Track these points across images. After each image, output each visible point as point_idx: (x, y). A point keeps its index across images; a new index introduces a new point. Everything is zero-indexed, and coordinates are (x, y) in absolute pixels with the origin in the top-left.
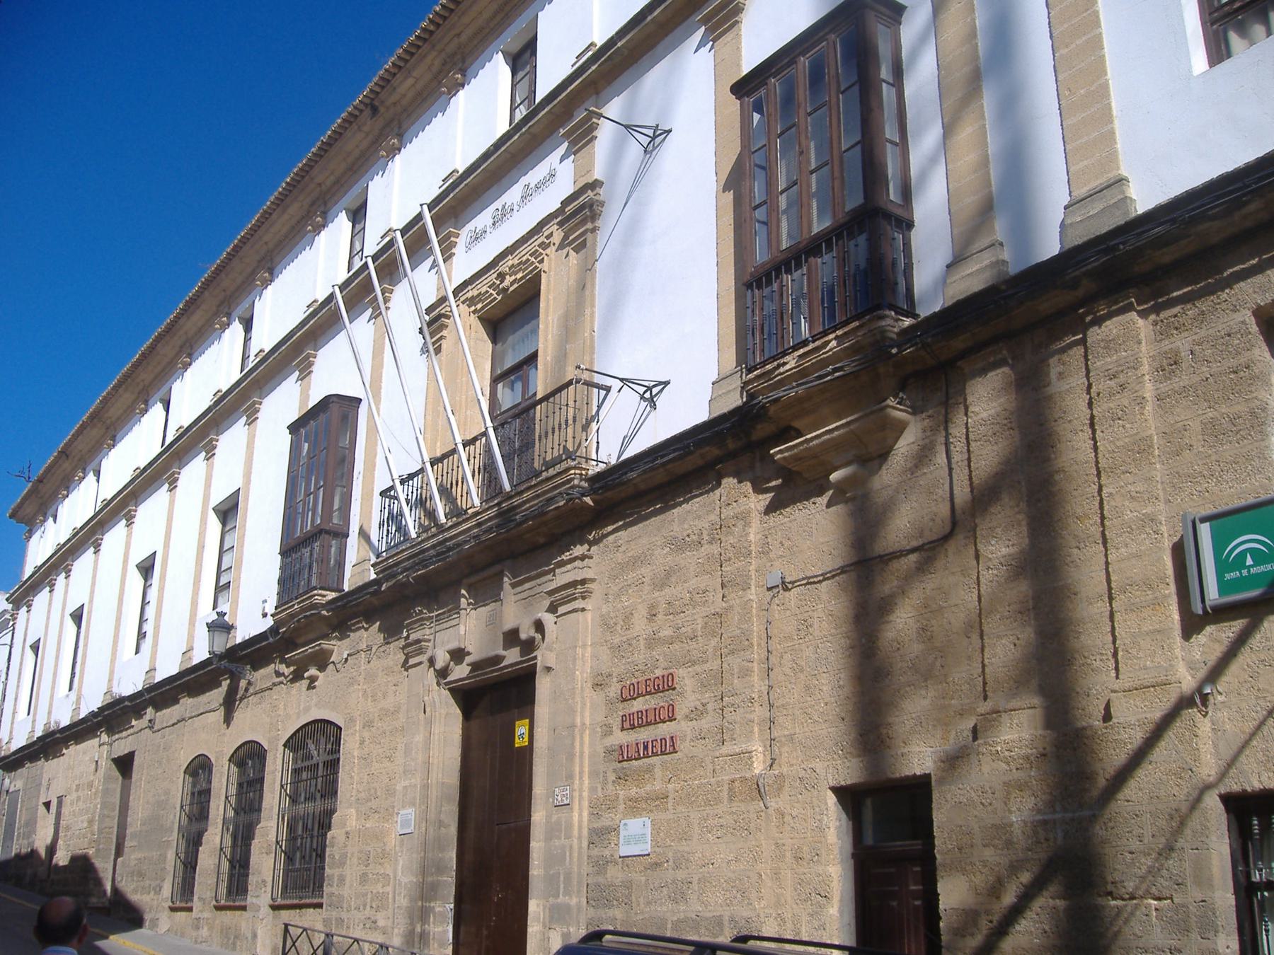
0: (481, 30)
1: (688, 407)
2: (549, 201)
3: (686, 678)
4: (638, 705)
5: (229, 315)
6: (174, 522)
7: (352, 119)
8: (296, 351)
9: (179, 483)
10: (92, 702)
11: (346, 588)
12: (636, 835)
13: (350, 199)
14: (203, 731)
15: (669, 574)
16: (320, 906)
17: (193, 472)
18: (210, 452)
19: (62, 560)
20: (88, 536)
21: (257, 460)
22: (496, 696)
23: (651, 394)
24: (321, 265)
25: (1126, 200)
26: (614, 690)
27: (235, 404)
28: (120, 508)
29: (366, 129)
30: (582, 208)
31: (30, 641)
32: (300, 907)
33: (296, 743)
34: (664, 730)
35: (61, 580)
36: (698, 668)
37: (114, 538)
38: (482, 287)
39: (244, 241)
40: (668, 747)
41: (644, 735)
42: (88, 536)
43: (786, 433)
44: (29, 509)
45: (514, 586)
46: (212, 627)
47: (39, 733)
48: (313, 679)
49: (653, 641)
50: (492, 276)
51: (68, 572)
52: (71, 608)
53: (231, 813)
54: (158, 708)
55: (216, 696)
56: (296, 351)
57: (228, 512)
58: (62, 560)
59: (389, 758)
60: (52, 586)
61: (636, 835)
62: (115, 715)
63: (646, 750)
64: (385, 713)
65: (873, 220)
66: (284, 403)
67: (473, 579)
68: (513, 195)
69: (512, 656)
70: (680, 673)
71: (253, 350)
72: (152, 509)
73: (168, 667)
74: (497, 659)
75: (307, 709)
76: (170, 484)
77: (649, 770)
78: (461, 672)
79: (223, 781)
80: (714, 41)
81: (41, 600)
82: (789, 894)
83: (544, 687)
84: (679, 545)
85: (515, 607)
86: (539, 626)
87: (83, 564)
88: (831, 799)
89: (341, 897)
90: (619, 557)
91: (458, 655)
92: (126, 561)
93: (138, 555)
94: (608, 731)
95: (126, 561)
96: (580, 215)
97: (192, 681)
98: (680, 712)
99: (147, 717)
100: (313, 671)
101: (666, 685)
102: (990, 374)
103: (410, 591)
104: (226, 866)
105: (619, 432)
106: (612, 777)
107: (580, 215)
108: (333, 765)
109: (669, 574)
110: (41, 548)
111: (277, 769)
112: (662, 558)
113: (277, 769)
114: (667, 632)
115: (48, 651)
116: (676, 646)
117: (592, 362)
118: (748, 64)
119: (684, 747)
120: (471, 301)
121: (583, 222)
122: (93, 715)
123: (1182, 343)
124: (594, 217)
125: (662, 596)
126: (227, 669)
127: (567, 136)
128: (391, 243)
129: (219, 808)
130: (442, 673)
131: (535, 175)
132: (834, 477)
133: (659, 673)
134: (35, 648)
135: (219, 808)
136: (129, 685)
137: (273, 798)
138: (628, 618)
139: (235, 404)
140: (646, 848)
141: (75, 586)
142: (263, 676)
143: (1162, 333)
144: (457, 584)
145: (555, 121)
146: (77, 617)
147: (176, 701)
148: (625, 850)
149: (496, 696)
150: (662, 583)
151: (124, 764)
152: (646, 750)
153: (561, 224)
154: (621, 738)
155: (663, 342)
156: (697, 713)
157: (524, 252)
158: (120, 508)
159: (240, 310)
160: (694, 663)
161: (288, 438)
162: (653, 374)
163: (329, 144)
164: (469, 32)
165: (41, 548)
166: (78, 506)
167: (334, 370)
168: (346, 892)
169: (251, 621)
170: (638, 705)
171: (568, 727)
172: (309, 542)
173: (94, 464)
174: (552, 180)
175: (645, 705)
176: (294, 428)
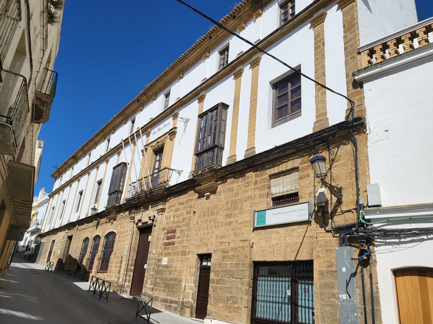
0: (160, 88)
1: (185, 177)
2: (167, 129)
3: (178, 230)
4: (169, 235)
5: (105, 138)
6: (88, 183)
7: (133, 102)
8: (117, 150)
9: (121, 154)
10: (65, 223)
11: (121, 204)
12: (165, 261)
13: (132, 118)
14: (90, 231)
15: (178, 209)
16: (107, 272)
17: (94, 172)
18: (98, 168)
19: (62, 188)
20: (69, 183)
21: (106, 172)
22: (145, 230)
23: (179, 173)
24: (123, 132)
25: (255, 152)
26: (166, 231)
27: (104, 159)
28: (77, 178)
29: (136, 104)
30: (173, 132)
31: (52, 207)
32: (103, 272)
33: (107, 236)
34: (173, 240)
35: (61, 192)
36: (180, 228)
37: (75, 184)
38: (153, 144)
39: (109, 123)
40: (173, 244)
41: (170, 241)
42: (69, 183)
43: (200, 185)
44: (56, 175)
45: (151, 208)
46: (92, 209)
47: (51, 229)
48: (112, 223)
49: (174, 222)
50: (156, 142)
51: (63, 191)
52: (63, 200)
53: (92, 251)
54: (79, 225)
55: (95, 222)
56: (117, 150)
57: (100, 183)
58: (62, 188)
59: (125, 241)
60: (59, 194)
61: (165, 261)
62: (70, 226)
63: (169, 244)
64: (125, 231)
65: (216, 148)
66: (114, 161)
67: (144, 205)
68: (161, 126)
69: (150, 222)
70: (177, 229)
71: (109, 148)
72: (84, 179)
73: (83, 217)
74: (147, 222)
75: (110, 229)
76: (147, 135)
77: (170, 248)
78: (140, 224)
79: (91, 243)
80: (314, 28)
81: (56, 196)
82: (188, 274)
83: (154, 229)
84: (181, 204)
85: (151, 212)
86: (154, 217)
87: (67, 189)
88: (196, 256)
89: (111, 270)
90: (170, 205)
91: (140, 221)
92: (77, 191)
93: (79, 190)
94: (164, 240)
95: (77, 191)
96: (172, 133)
97: (87, 220)
98: (176, 237)
99: (77, 227)
100: (112, 221)
101: (174, 231)
102: (228, 181)
103: (137, 204)
104: (89, 262)
105: (174, 180)
106: (163, 249)
107: (172, 133)
108: (114, 241)
109: (178, 209)
110: (57, 184)
111: (102, 241)
112: (177, 206)
113: (102, 241)
114: (176, 221)
115: (56, 209)
116: (177, 224)
117: (170, 165)
118: (205, 109)
119: (176, 244)
120: (152, 147)
121: (173, 135)
122: (64, 226)
123: (258, 179)
124: (175, 135)
125: (176, 213)
126: (96, 217)
127: (172, 116)
128: (139, 130)
129: (89, 249)
130: (137, 224)
131: (166, 122)
132: (205, 194)
133: (174, 229)
134: (53, 208)
135: (89, 249)
136: (74, 219)
137: (100, 248)
138: (170, 217)
139: (104, 159)
140: (166, 263)
141: (64, 195)
142: (103, 220)
143: (257, 176)
144: (141, 206)
145: (171, 112)
146: (64, 202)
147: (83, 224)
148: (163, 264)
149: (145, 230)
150: (176, 211)
151: (70, 238)
152: (169, 244)
153: (169, 134)
154: (166, 241)
155: (181, 164)
156: (179, 237)
157: (162, 138)
158: (77, 178)
159: (107, 138)
160: (179, 227)
161: (112, 170)
162: (180, 170)
163: (128, 106)
164: (158, 88)
165: (57, 184)
166: (67, 176)
167: (126, 155)
168: (112, 269)
169: (101, 208)
170: (169, 235)
171: (156, 238)
172: (115, 192)
173: (72, 167)
174: (167, 125)
175: (171, 233)
176: (114, 168)
